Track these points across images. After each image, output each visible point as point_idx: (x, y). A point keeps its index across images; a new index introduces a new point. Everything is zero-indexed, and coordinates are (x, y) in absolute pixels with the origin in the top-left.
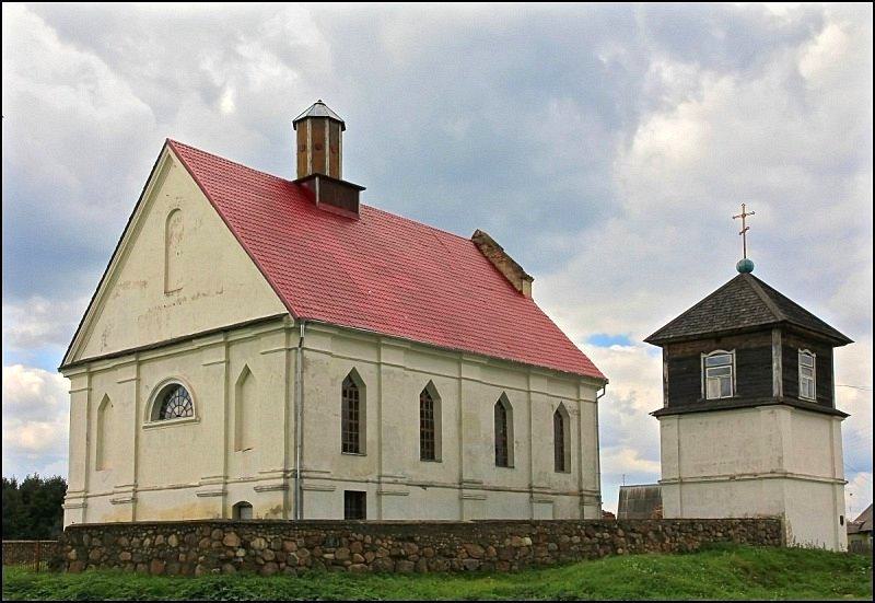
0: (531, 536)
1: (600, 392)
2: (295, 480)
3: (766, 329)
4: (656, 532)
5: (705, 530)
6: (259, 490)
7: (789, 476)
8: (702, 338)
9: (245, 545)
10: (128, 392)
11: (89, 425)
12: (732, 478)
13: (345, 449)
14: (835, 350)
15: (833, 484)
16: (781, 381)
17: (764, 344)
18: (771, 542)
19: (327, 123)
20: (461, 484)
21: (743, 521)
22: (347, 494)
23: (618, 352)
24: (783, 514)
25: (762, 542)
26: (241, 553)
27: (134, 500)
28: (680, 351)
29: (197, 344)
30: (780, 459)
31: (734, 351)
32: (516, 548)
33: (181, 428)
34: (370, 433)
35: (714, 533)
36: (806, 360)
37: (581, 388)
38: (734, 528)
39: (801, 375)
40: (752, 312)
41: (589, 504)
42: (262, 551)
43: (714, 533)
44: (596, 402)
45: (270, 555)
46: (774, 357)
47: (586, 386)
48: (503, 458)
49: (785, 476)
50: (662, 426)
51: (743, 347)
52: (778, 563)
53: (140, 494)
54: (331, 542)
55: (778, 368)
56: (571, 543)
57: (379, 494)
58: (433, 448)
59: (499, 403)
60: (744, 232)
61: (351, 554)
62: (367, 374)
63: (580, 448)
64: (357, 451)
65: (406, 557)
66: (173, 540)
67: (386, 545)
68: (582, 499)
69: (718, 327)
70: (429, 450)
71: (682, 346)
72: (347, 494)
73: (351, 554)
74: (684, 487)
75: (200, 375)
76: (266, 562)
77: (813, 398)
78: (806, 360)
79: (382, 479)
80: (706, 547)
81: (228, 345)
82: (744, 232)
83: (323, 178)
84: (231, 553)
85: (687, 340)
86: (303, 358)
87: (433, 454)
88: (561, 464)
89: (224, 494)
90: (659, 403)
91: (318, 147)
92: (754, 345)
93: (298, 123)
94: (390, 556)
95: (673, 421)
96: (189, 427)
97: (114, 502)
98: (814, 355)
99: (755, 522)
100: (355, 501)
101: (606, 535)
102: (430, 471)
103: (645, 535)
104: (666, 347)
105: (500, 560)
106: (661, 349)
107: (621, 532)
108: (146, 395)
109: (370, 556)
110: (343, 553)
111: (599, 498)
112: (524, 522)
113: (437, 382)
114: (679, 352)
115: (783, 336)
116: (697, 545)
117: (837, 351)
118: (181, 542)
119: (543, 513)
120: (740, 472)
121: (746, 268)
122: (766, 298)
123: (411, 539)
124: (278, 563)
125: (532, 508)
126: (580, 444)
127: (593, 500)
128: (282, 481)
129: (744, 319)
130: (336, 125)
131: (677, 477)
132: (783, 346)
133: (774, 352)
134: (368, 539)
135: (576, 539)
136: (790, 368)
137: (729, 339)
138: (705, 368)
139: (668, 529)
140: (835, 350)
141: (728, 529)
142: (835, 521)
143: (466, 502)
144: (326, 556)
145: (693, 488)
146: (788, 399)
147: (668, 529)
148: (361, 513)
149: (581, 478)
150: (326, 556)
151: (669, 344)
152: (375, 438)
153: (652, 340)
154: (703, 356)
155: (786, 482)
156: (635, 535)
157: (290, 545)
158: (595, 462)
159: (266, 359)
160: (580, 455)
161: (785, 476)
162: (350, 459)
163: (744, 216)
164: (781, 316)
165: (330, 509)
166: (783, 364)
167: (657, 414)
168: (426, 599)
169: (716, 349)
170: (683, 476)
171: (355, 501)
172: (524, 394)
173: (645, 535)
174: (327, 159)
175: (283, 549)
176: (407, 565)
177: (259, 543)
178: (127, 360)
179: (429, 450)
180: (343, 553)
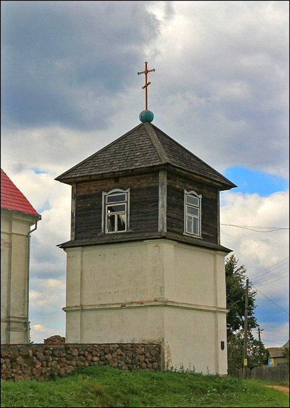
1: (33, 227)
3: (153, 171)
4: (26, 357)
5: (79, 355)
7: (169, 304)
8: (102, 178)
15: (215, 312)
16: (165, 218)
17: (153, 185)
18: (150, 365)
21: (121, 346)
22: (222, 342)
24: (163, 339)
25: (141, 367)
28: (86, 189)
30: (162, 288)
31: (128, 190)
35: (90, 357)
36: (192, 201)
37: (13, 223)
38: (111, 352)
39: (187, 214)
40: (144, 155)
41: (15, 329)
43: (90, 357)
44: (28, 236)
46: (160, 196)
47: (18, 220)
49: (165, 305)
50: (68, 257)
51: (136, 187)
52: (137, 386)
55: (163, 206)
60: (146, 87)
63: (9, 278)
66: (31, 352)
68: (9, 325)
69: (116, 169)
71: (85, 182)
74: (85, 314)
77: (199, 235)
78: (192, 201)
79: (11, 319)
80: (79, 370)
81: (82, 251)
82: (146, 87)
85: (90, 180)
90: (67, 236)
92: (145, 185)
95: (77, 252)
98: (200, 196)
99: (133, 346)
103: (13, 360)
104: (75, 185)
106: (69, 187)
111: (26, 324)
114: (83, 191)
115: (168, 178)
116: (70, 369)
117: (224, 195)
120: (129, 300)
121: (147, 118)
122: (158, 144)
126: (10, 274)
127: (20, 326)
129: (137, 161)
131: (78, 304)
132: (168, 187)
133: (160, 192)
136: (176, 204)
137: (125, 179)
138: (105, 205)
139: (40, 354)
141: (106, 354)
142: (216, 346)
145: (92, 315)
147: (40, 354)
151: (77, 183)
153: (62, 179)
154: (104, 194)
155: (166, 310)
158: (24, 290)
160: (9, 284)
161: (165, 305)
163: (146, 72)
164: (165, 159)
166: (168, 203)
167: (64, 246)
168: (65, 406)
169: (111, 190)
170: (84, 303)
172: (24, 238)
173: (13, 360)
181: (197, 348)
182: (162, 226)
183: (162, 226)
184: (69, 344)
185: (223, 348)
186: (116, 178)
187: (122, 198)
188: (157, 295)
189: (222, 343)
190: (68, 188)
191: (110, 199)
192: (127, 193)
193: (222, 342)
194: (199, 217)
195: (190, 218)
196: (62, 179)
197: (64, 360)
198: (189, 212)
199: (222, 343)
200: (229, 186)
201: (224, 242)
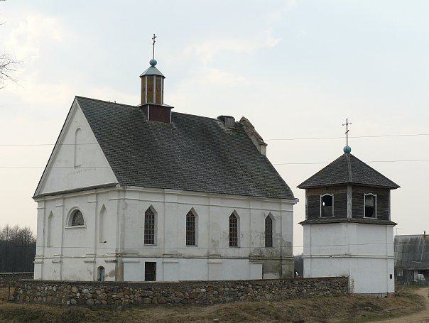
0: (205, 288)
2: (119, 258)
3: (344, 186)
6: (106, 262)
9: (80, 292)
10: (61, 211)
11: (45, 225)
13: (231, 245)
22: (147, 264)
26: (78, 294)
27: (61, 262)
32: (198, 293)
33: (79, 230)
45: (90, 295)
53: (65, 260)
60: (347, 133)
62: (157, 207)
65: (148, 297)
66: (55, 289)
70: (191, 239)
72: (147, 264)
75: (86, 206)
82: (347, 133)
87: (194, 242)
89: (94, 262)
90: (304, 218)
91: (150, 90)
93: (142, 77)
95: (308, 227)
96: (82, 230)
100: (150, 269)
102: (192, 251)
107: (250, 286)
108: (66, 213)
109: (132, 296)
110: (121, 295)
112: (203, 281)
118: (57, 290)
120: (334, 254)
121: (347, 151)
128: (115, 259)
134: (131, 289)
152: (162, 237)
159: (111, 202)
161: (350, 257)
162: (149, 246)
163: (347, 124)
165: (135, 274)
171: (150, 269)
176: (148, 300)
177: (85, 291)
178: (59, 197)
179: (191, 239)
181: (373, 278)
182: (349, 215)
183: (349, 215)
184: (46, 282)
185: (391, 278)
189: (391, 276)
199: (391, 276)
200: (396, 187)
201: (393, 219)
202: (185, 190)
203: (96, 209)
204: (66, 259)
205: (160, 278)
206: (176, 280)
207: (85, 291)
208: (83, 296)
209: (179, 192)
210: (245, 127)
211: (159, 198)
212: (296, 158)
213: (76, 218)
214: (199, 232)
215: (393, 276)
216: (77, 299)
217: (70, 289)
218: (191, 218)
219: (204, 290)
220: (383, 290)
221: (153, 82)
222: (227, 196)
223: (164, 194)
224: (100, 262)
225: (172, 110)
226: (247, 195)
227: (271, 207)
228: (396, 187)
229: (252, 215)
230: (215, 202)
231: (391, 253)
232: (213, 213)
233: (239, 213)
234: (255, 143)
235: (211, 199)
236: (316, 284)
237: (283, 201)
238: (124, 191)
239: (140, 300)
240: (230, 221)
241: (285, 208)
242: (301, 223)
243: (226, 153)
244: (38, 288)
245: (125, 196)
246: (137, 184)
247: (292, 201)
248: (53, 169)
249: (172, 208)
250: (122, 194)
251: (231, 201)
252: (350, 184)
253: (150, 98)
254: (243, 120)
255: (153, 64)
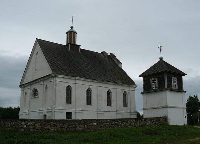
3: (163, 73)
6: (47, 112)
9: (26, 125)
10: (29, 90)
12: (157, 108)
13: (108, 105)
14: (183, 76)
15: (183, 108)
19: (72, 32)
20: (98, 110)
22: (67, 113)
23: (53, 84)
24: (168, 116)
26: (25, 126)
29: (39, 80)
32: (92, 126)
34: (128, 105)
42: (30, 126)
48: (109, 103)
54: (46, 124)
56: (106, 125)
57: (75, 113)
58: (90, 102)
59: (108, 91)
61: (51, 127)
62: (72, 86)
64: (70, 103)
65: (64, 128)
66: (132, 120)
67: (59, 125)
70: (89, 102)
73: (51, 127)
76: (31, 128)
77: (177, 88)
81: (44, 81)
83: (71, 44)
84: (23, 126)
86: (56, 83)
87: (90, 103)
88: (125, 105)
91: (70, 38)
94: (60, 127)
95: (145, 95)
96: (38, 98)
97: (26, 114)
100: (69, 115)
101: (116, 122)
105: (88, 128)
107: (120, 122)
109: (55, 127)
110: (49, 127)
113: (91, 87)
117: (183, 77)
118: (15, 124)
119: (120, 117)
121: (161, 59)
122: (163, 63)
123: (66, 124)
124: (34, 128)
125: (117, 116)
130: (74, 33)
134: (55, 124)
135: (108, 123)
136: (170, 81)
140: (183, 76)
143: (98, 114)
144: (45, 127)
146: (168, 88)
148: (71, 118)
149: (130, 108)
150: (45, 127)
153: (140, 76)
156: (124, 122)
157: (36, 125)
162: (68, 105)
163: (160, 47)
166: (167, 81)
171: (69, 115)
174: (72, 40)
175: (35, 125)
179: (89, 102)
180: (49, 127)
181: (178, 117)
182: (166, 86)
183: (166, 86)
185: (185, 117)
186: (154, 75)
187: (155, 80)
188: (166, 105)
189: (185, 116)
190: (142, 78)
191: (153, 80)
192: (156, 79)
193: (67, 113)
194: (177, 83)
195: (174, 84)
196: (140, 76)
197: (140, 122)
198: (173, 82)
199: (185, 116)
200: (185, 74)
201: (184, 89)
202: (86, 78)
203: (43, 87)
204: (31, 111)
205: (73, 118)
206: (80, 119)
207: (29, 124)
208: (28, 127)
209: (83, 79)
210: (112, 57)
211: (73, 81)
212: (134, 69)
213: (35, 92)
214: (93, 99)
215: (186, 117)
216: (24, 129)
217: (21, 123)
218: (89, 91)
219: (95, 124)
220: (183, 124)
221: (71, 35)
222: (106, 82)
223: (75, 80)
224: (45, 113)
225: (81, 47)
226: (115, 82)
227: (126, 89)
228: (185, 74)
229: (117, 91)
230: (100, 85)
231: (185, 106)
232: (100, 90)
233: (111, 90)
234: (117, 62)
235: (98, 83)
236: (153, 121)
237: (131, 86)
238: (56, 77)
239: (60, 129)
240: (107, 94)
241: (131, 89)
242: (141, 93)
243: (105, 67)
244: (7, 123)
245: (53, 79)
246: (63, 74)
247: (135, 86)
248: (27, 72)
249: (80, 86)
250: (54, 78)
251: (106, 85)
252: (166, 71)
253: (70, 40)
254: (111, 54)
255: (72, 28)
